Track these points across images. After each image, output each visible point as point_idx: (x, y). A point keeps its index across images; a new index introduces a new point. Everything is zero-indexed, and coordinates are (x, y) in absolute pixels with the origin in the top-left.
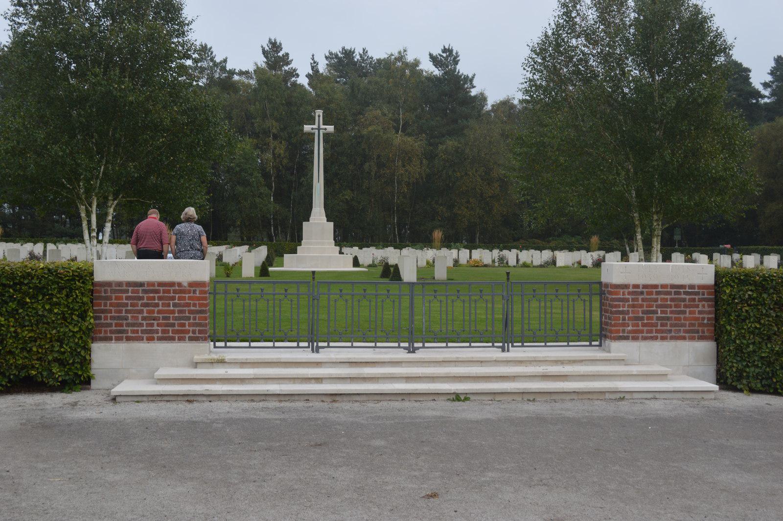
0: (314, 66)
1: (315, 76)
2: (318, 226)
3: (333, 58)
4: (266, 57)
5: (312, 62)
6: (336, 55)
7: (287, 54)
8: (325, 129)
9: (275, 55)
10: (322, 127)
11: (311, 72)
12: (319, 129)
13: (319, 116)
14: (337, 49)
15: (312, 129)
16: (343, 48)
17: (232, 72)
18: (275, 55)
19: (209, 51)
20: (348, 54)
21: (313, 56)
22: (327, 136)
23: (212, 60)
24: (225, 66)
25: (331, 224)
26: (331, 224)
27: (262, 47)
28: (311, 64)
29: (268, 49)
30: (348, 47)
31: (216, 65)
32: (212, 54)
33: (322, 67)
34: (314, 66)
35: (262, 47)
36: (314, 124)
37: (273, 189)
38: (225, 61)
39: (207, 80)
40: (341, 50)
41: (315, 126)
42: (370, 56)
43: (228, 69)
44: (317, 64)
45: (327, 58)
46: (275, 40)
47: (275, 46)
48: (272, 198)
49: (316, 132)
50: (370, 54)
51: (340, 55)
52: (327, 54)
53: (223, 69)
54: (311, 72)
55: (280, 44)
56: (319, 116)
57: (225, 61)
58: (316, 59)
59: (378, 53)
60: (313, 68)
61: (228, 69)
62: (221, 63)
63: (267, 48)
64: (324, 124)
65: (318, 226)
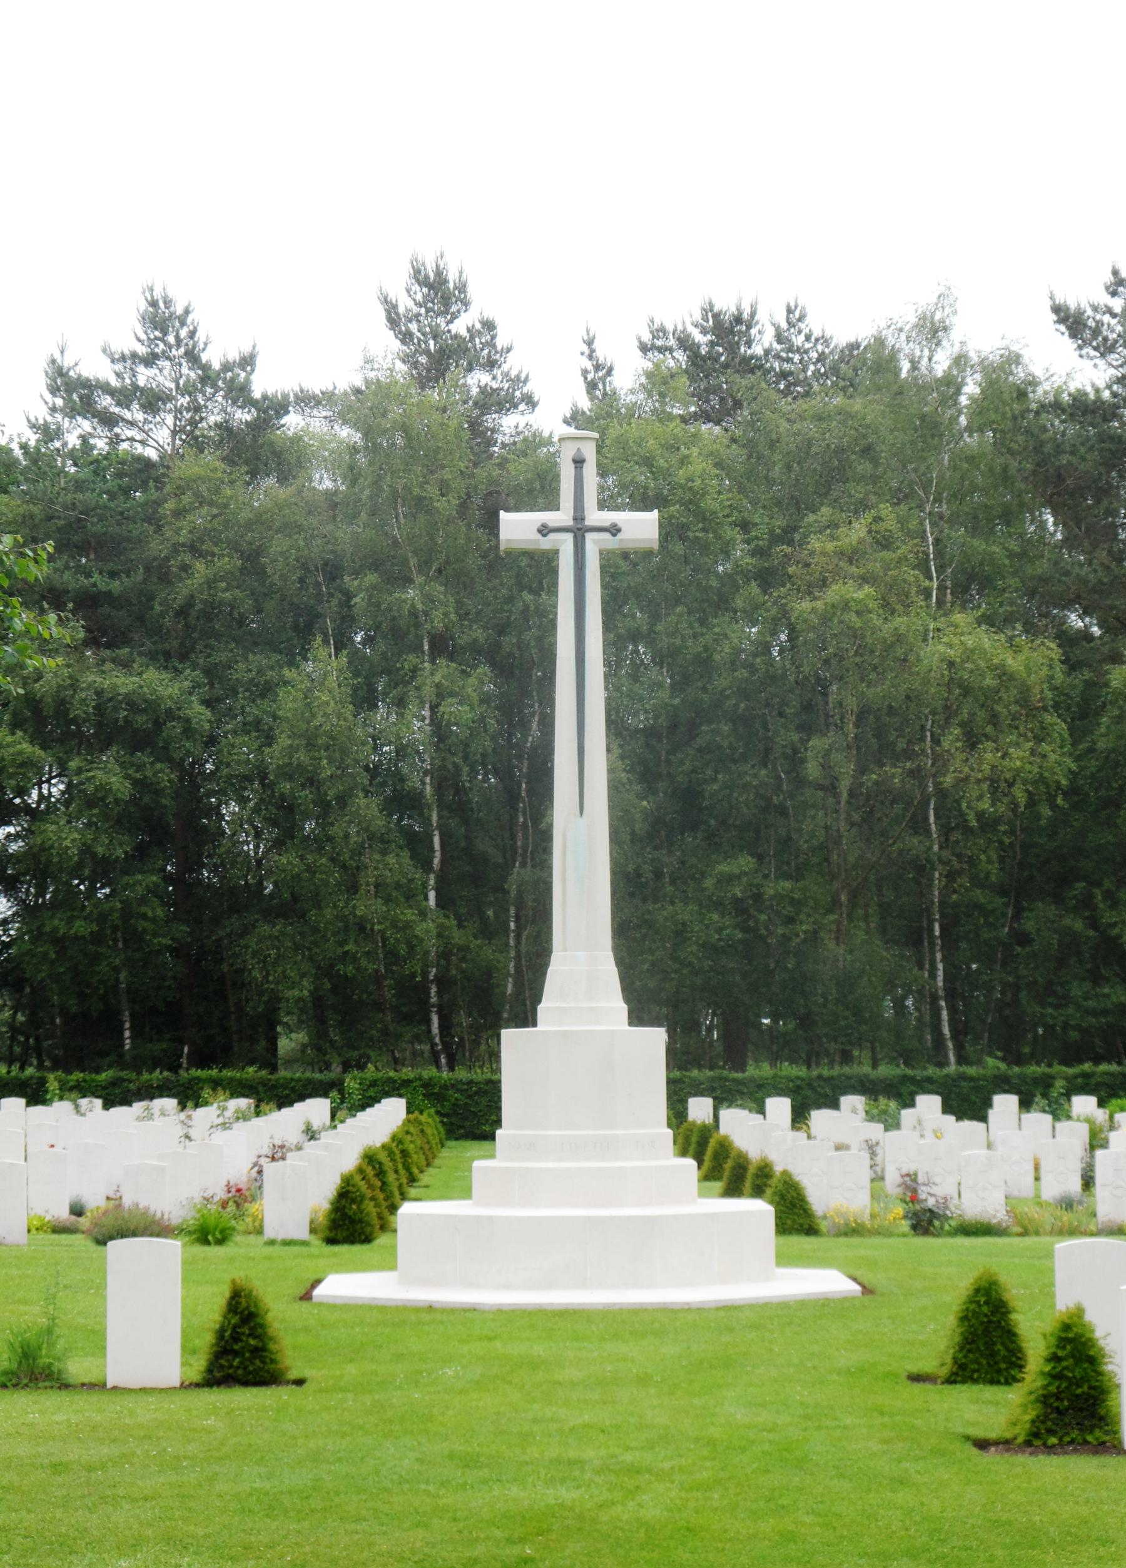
0: (597, 378)
1: (602, 414)
2: (583, 1042)
3: (671, 350)
4: (406, 337)
5: (589, 365)
6: (684, 342)
7: (489, 326)
8: (614, 530)
9: (440, 334)
10: (595, 516)
11: (585, 404)
12: (579, 531)
13: (579, 462)
14: (682, 314)
15: (544, 530)
16: (708, 310)
17: (276, 407)
18: (440, 334)
19: (183, 323)
20: (729, 329)
21: (590, 343)
22: (621, 569)
23: (192, 356)
24: (248, 381)
25: (656, 1038)
26: (656, 1038)
27: (386, 301)
28: (585, 372)
29: (410, 304)
30: (726, 305)
31: (207, 377)
32: (192, 334)
33: (628, 376)
34: (597, 378)
35: (386, 301)
36: (557, 509)
37: (436, 861)
38: (248, 362)
39: (174, 433)
40: (698, 316)
41: (562, 516)
42: (817, 333)
43: (257, 395)
44: (609, 372)
45: (644, 349)
46: (439, 273)
47: (440, 292)
48: (432, 895)
49: (565, 544)
50: (815, 324)
51: (699, 337)
52: (647, 337)
53: (239, 393)
54: (585, 404)
55: (462, 287)
56: (579, 462)
57: (248, 362)
58: (600, 354)
59: (844, 320)
60: (591, 386)
61: (257, 395)
62: (227, 367)
63: (405, 304)
64: (602, 505)
65: (583, 1042)
